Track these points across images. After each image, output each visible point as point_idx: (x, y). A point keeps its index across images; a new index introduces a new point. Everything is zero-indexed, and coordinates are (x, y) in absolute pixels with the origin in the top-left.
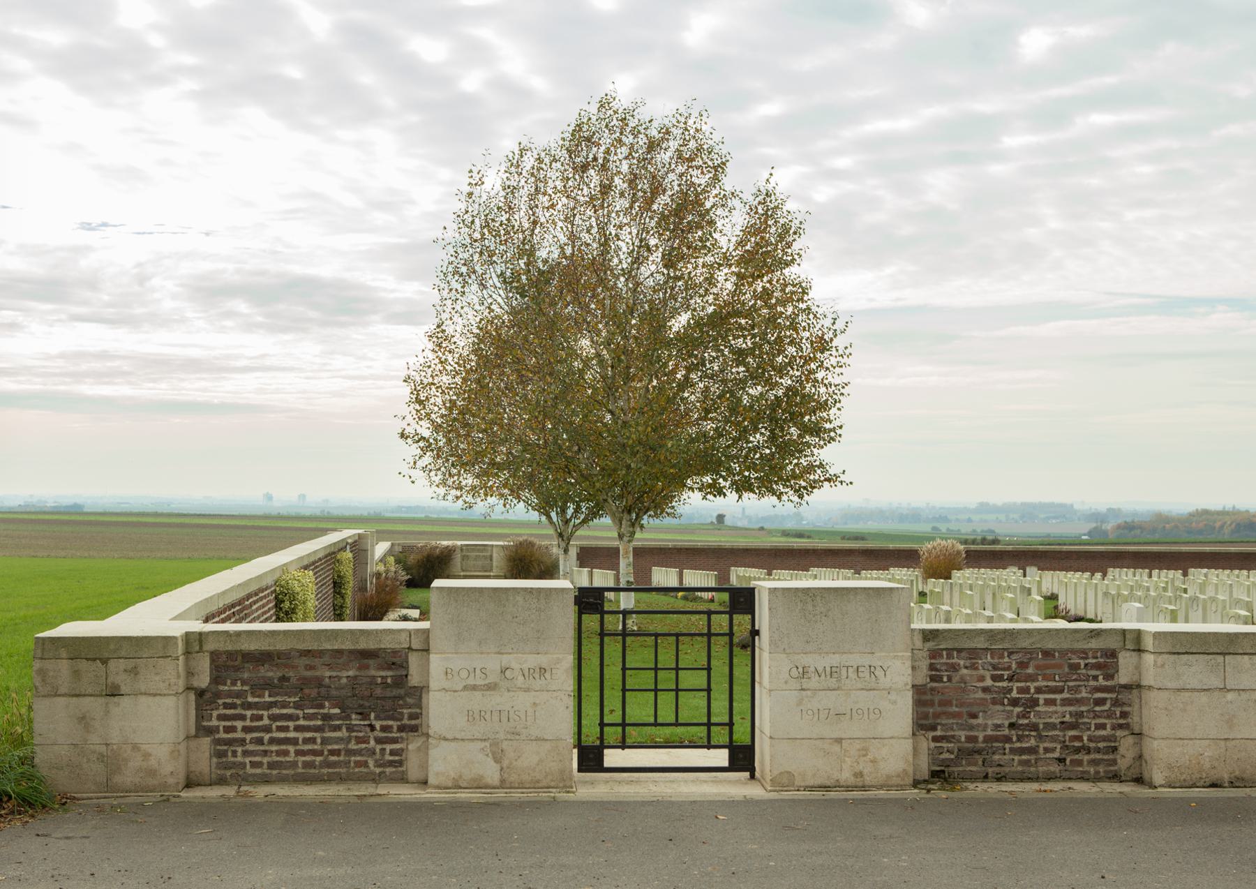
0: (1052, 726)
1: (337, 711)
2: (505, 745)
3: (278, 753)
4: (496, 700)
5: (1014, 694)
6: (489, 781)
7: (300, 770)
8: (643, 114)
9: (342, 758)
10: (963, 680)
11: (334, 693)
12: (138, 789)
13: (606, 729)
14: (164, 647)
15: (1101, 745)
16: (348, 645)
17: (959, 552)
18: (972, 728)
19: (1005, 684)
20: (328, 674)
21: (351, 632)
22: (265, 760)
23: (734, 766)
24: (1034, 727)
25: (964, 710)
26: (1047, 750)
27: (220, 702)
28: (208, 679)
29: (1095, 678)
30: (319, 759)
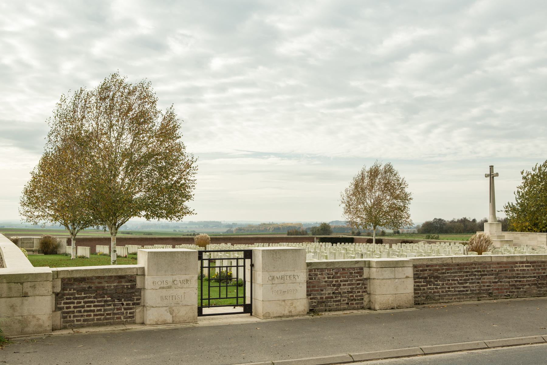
0: (344, 293)
1: (110, 299)
2: (174, 308)
3: (87, 316)
4: (172, 292)
5: (334, 283)
6: (168, 321)
7: (95, 322)
8: (126, 81)
9: (111, 316)
10: (319, 279)
11: (109, 292)
12: (34, 333)
13: (203, 301)
14: (47, 277)
15: (359, 298)
16: (114, 274)
17: (208, 238)
18: (321, 294)
19: (331, 280)
20: (106, 285)
21: (116, 269)
22: (82, 319)
23: (245, 312)
24: (340, 293)
25: (319, 289)
26: (343, 300)
27: (65, 297)
28: (60, 289)
29: (357, 276)
30: (102, 317)
